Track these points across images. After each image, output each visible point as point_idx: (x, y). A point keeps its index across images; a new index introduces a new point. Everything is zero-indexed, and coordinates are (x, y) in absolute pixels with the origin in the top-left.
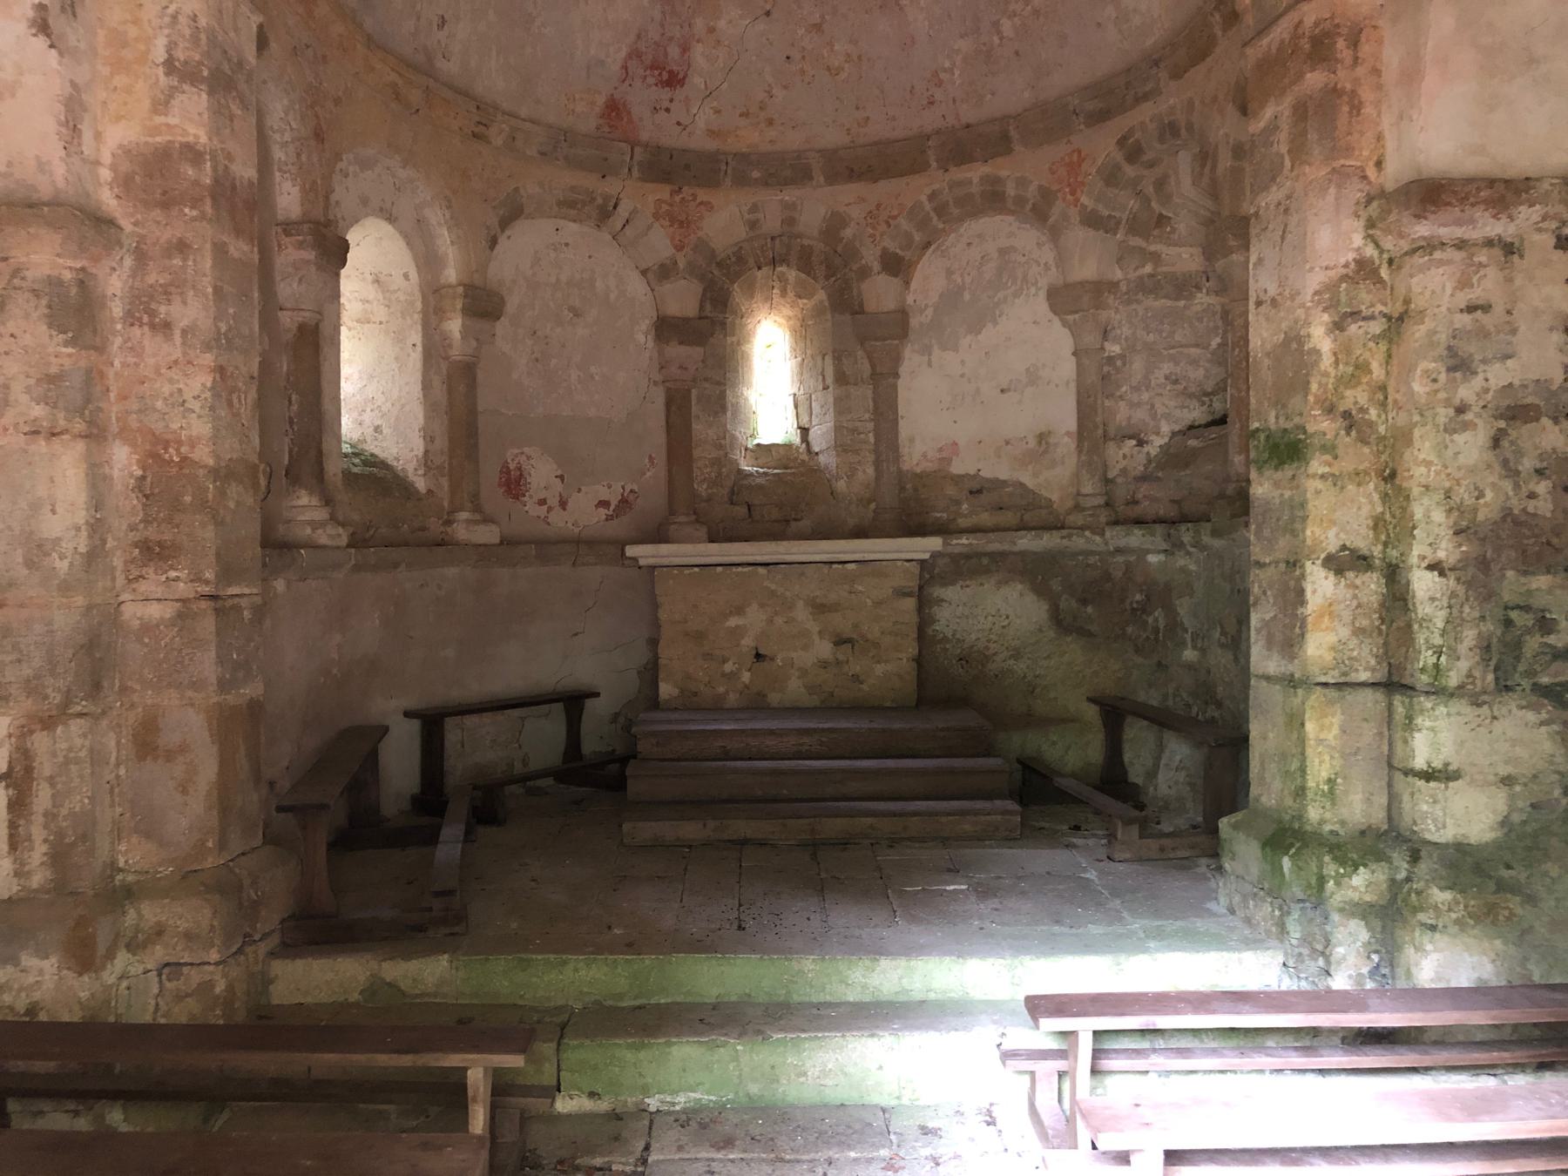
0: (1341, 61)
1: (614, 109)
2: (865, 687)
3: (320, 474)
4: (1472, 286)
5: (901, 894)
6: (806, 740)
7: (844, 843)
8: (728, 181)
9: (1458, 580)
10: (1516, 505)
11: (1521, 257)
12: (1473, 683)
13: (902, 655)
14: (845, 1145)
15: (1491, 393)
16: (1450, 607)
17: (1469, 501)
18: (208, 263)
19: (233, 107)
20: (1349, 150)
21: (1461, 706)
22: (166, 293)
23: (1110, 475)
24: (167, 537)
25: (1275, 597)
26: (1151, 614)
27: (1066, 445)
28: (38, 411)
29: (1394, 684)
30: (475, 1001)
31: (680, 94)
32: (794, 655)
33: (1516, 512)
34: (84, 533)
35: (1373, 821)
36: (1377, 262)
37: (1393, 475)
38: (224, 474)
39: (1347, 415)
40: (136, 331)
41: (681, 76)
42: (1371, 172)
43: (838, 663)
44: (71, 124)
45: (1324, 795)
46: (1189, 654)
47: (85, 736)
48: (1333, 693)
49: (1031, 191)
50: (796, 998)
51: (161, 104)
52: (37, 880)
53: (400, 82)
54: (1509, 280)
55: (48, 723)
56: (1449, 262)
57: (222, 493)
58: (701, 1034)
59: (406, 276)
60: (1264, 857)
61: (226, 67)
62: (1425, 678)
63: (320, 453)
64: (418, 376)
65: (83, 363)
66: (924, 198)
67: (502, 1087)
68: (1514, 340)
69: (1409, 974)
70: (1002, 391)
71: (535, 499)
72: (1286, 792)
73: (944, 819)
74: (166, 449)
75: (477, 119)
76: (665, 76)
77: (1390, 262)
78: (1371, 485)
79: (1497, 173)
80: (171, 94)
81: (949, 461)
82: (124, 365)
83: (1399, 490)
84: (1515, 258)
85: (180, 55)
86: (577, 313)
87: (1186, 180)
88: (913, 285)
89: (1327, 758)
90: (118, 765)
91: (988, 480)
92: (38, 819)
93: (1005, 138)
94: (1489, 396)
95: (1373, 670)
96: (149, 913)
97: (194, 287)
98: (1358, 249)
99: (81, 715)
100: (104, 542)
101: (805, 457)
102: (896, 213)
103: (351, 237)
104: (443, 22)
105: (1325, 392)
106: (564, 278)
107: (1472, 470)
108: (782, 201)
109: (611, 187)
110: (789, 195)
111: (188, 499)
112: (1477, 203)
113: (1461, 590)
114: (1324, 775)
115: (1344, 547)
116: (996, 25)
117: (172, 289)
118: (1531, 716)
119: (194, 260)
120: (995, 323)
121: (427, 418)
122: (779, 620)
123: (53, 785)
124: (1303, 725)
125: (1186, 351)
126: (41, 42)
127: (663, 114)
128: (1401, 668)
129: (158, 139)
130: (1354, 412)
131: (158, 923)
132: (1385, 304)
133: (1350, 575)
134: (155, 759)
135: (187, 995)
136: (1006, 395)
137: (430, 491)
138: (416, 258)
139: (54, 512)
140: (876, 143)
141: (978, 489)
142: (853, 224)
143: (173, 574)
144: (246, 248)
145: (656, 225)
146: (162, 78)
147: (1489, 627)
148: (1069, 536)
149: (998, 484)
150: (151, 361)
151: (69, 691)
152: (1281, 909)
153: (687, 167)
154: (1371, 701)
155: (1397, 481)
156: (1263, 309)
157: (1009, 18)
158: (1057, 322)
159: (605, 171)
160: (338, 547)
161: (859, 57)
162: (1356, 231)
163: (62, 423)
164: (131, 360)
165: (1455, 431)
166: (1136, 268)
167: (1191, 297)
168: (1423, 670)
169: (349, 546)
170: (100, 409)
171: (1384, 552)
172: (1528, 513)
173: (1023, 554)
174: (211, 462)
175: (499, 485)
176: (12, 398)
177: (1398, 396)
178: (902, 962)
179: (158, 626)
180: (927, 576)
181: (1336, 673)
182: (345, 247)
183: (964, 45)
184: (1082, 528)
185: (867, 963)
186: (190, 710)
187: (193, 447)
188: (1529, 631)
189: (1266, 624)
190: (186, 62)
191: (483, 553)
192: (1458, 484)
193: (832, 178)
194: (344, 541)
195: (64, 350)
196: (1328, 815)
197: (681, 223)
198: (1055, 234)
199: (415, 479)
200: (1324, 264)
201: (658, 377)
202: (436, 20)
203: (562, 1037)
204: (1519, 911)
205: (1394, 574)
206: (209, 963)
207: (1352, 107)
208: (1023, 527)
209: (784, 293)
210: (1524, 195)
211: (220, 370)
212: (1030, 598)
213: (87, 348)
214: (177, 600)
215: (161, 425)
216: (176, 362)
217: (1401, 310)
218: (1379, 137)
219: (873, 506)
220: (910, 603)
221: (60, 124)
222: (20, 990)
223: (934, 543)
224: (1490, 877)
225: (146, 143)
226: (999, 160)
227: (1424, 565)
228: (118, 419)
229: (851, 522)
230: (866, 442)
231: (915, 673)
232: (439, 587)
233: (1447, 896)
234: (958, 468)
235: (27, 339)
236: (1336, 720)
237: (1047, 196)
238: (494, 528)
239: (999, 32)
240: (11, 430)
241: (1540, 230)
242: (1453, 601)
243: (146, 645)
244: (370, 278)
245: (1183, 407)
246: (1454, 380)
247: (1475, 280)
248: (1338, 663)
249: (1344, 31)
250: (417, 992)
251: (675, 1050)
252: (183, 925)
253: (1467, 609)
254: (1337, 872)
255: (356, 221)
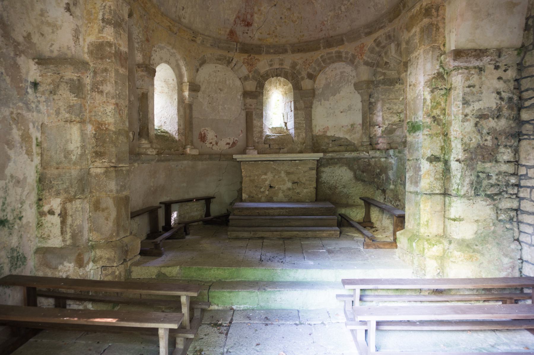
0: (433, 16)
1: (232, 33)
2: (301, 196)
3: (148, 134)
4: (470, 80)
5: (307, 252)
6: (281, 211)
7: (290, 238)
8: (264, 53)
9: (464, 164)
10: (481, 143)
11: (484, 72)
12: (468, 194)
13: (312, 187)
14: (286, 320)
15: (475, 111)
16: (462, 172)
17: (468, 142)
18: (113, 75)
19: (121, 32)
20: (435, 41)
21: (465, 200)
22: (102, 83)
23: (371, 136)
24: (102, 150)
25: (413, 169)
26: (381, 175)
27: (359, 128)
28: (67, 115)
29: (445, 194)
30: (186, 279)
31: (251, 28)
32: (281, 186)
33: (481, 145)
34: (80, 149)
35: (439, 233)
36: (443, 73)
37: (447, 134)
38: (118, 133)
39: (434, 117)
40: (94, 93)
41: (251, 23)
42: (442, 48)
43: (293, 189)
44: (76, 36)
45: (425, 225)
46: (392, 187)
47: (80, 204)
48: (429, 196)
49: (350, 55)
50: (275, 280)
51: (101, 31)
52: (68, 243)
53: (171, 25)
54: (481, 78)
55: (71, 201)
56: (463, 73)
57: (117, 138)
58: (248, 289)
59: (173, 80)
60: (409, 242)
61: (119, 20)
62: (454, 192)
63: (148, 128)
64: (176, 107)
65: (79, 102)
66: (319, 57)
67: (193, 303)
68: (482, 95)
69: (447, 275)
70: (341, 112)
71: (209, 142)
72: (415, 224)
73: (318, 232)
74: (102, 126)
75: (193, 36)
76: (246, 23)
77: (447, 73)
78: (441, 138)
79: (477, 47)
80: (103, 28)
81: (326, 132)
82: (90, 103)
83: (449, 138)
84: (483, 72)
85: (106, 17)
86: (221, 90)
87: (393, 52)
88: (316, 82)
89: (426, 215)
90: (90, 212)
91: (337, 137)
92: (68, 226)
93: (342, 40)
94: (474, 112)
95: (440, 190)
96: (99, 253)
97: (109, 81)
98: (438, 70)
99: (79, 198)
100: (85, 151)
101: (286, 131)
102: (311, 61)
103: (157, 69)
104: (183, 8)
105: (428, 111)
106: (218, 80)
107: (469, 133)
108: (279, 58)
109: (231, 55)
110: (281, 56)
111: (108, 140)
112: (471, 56)
113: (465, 167)
114: (426, 220)
115: (432, 155)
116: (340, 8)
117: (104, 82)
118: (484, 203)
119: (110, 74)
120: (339, 93)
121: (179, 119)
122: (277, 177)
123: (72, 217)
124: (420, 205)
125: (393, 101)
126: (68, 14)
127: (245, 34)
128: (448, 189)
129: (100, 40)
130: (436, 116)
131: (100, 255)
132: (446, 85)
133: (434, 163)
134: (99, 211)
135: (108, 275)
136: (342, 113)
137: (179, 140)
138: (176, 75)
139: (71, 143)
140: (305, 42)
141: (335, 140)
142: (299, 65)
143: (104, 160)
144: (124, 70)
145: (244, 66)
146: (101, 24)
147: (473, 177)
148: (359, 153)
149: (339, 139)
150: (98, 102)
151: (76, 192)
152: (412, 257)
153: (252, 49)
154: (440, 198)
155: (448, 136)
156: (411, 87)
157: (344, 6)
158: (356, 92)
159: (229, 50)
160: (153, 155)
161: (301, 18)
162: (437, 64)
163: (74, 119)
164: (92, 101)
165: (464, 122)
166: (379, 77)
167: (394, 85)
168: (454, 190)
169: (156, 155)
170: (84, 115)
171: (444, 156)
172: (485, 145)
173: (346, 158)
174: (114, 130)
175: (199, 138)
176: (60, 112)
177: (449, 112)
178: (305, 270)
179: (100, 175)
180: (319, 164)
181: (429, 191)
182: (154, 71)
183: (331, 14)
184: (363, 151)
185: (295, 271)
186: (108, 198)
187: (109, 125)
188: (484, 179)
189: (411, 177)
190: (108, 19)
191: (194, 158)
192: (465, 137)
193: (293, 52)
194: (154, 153)
195: (74, 98)
196: (426, 231)
197: (251, 65)
198: (356, 67)
199: (176, 136)
200: (428, 74)
201: (243, 108)
202: (181, 8)
203: (209, 289)
204: (479, 258)
205: (446, 162)
206: (114, 266)
207: (437, 29)
208: (347, 151)
209: (280, 84)
210: (485, 54)
211: (117, 104)
212: (348, 171)
213: (80, 98)
214: (105, 168)
215: (100, 119)
216: (104, 102)
217: (450, 87)
218: (444, 37)
219: (305, 145)
220: (314, 172)
221: (73, 36)
222: (64, 272)
223: (321, 155)
224: (471, 248)
225: (97, 41)
226: (341, 46)
227: (455, 160)
228: (89, 118)
229: (298, 149)
230: (303, 127)
231: (315, 192)
232: (182, 166)
233: (459, 253)
234: (329, 134)
235: (65, 96)
236: (429, 204)
237: (354, 56)
238: (198, 150)
239: (341, 10)
240: (60, 121)
241: (490, 64)
242: (463, 170)
243: (97, 180)
244: (163, 80)
245: (392, 117)
246: (464, 107)
247: (471, 78)
248: (430, 188)
249: (434, 7)
250: (171, 276)
251: (240, 293)
252: (107, 256)
253: (467, 172)
254: (428, 247)
255: (159, 64)
